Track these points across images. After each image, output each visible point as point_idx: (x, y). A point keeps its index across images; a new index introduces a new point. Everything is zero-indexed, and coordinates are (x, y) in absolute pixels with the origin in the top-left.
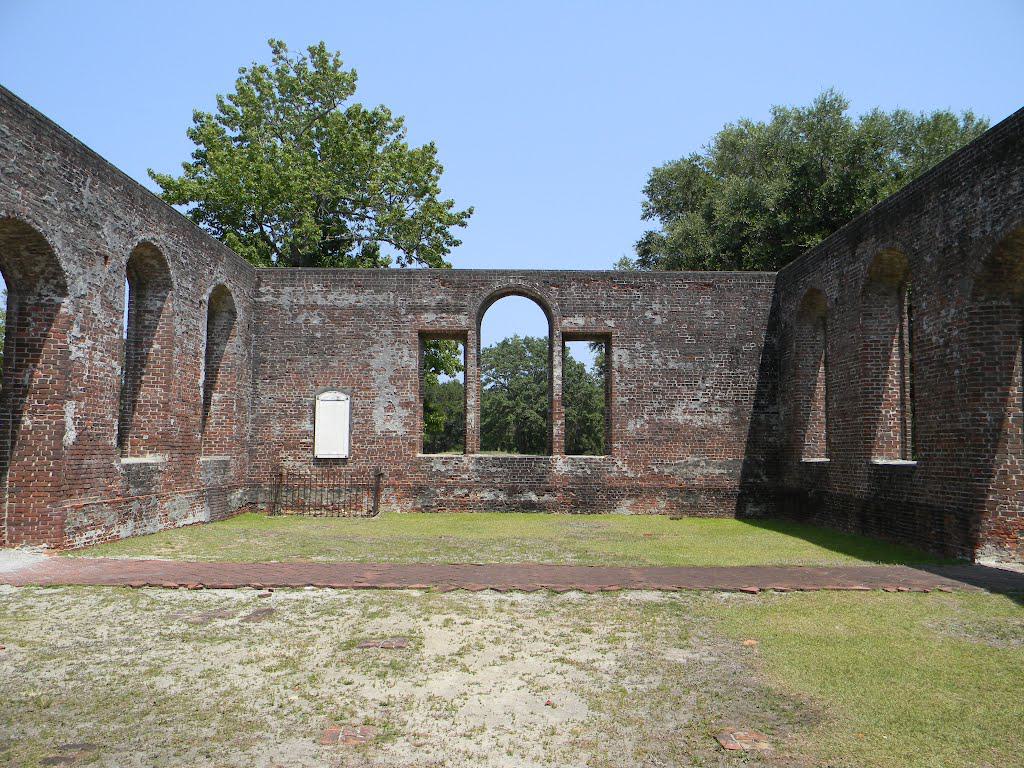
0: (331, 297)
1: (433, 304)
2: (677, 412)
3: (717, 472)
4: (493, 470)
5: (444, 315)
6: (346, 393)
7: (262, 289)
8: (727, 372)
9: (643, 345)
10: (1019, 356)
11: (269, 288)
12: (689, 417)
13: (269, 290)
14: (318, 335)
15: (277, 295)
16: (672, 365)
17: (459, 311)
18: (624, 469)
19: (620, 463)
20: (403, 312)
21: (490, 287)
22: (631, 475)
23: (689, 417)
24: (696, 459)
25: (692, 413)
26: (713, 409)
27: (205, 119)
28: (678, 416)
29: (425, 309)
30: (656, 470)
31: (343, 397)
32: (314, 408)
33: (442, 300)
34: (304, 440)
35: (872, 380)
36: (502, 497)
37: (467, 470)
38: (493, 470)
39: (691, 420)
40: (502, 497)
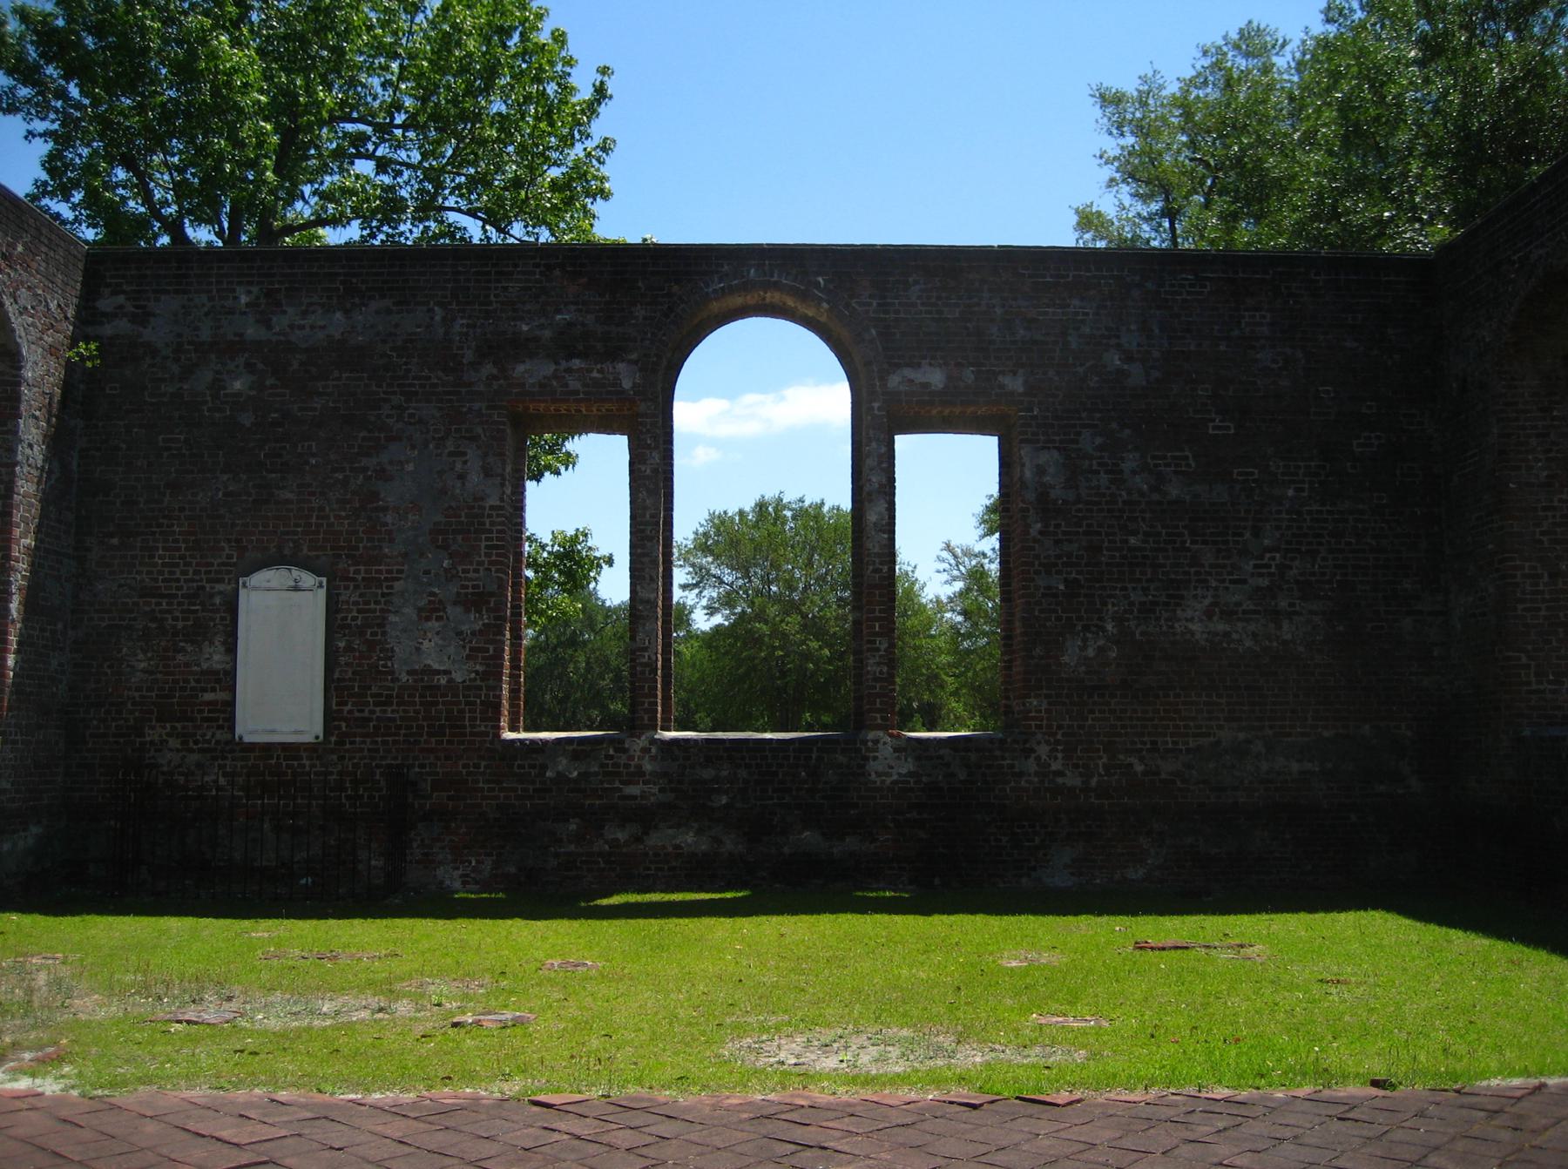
0: (281, 322)
1: (547, 333)
2: (1189, 613)
3: (1295, 767)
4: (708, 773)
5: (576, 363)
6: (317, 572)
7: (105, 304)
8: (1315, 508)
9: (1098, 441)
10: (599, 902)
11: (121, 299)
12: (1221, 627)
13: (121, 307)
14: (247, 420)
15: (142, 317)
16: (1174, 491)
17: (614, 354)
18: (1055, 766)
19: (1043, 751)
20: (469, 355)
21: (685, 292)
22: (1072, 780)
23: (1221, 627)
24: (1241, 736)
25: (1229, 614)
26: (1283, 604)
27: (887, 1145)
28: (1194, 621)
29: (522, 347)
30: (1139, 768)
31: (308, 579)
32: (232, 608)
33: (570, 324)
34: (209, 696)
35: (1152, 719)
36: (731, 844)
37: (640, 772)
38: (708, 773)
39: (1226, 634)
40: (731, 844)
